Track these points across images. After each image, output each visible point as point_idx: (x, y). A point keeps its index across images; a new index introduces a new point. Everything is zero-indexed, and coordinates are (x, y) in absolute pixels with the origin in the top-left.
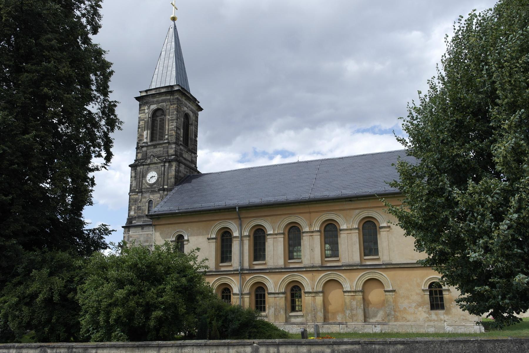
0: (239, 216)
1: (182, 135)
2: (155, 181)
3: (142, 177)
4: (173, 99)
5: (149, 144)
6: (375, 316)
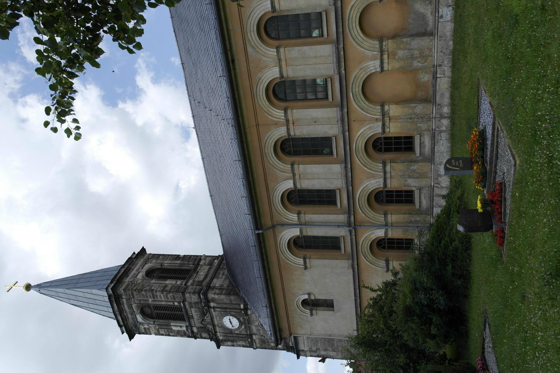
1: (174, 282)
2: (235, 319)
3: (232, 333)
4: (126, 295)
5: (187, 324)
6: (424, 16)
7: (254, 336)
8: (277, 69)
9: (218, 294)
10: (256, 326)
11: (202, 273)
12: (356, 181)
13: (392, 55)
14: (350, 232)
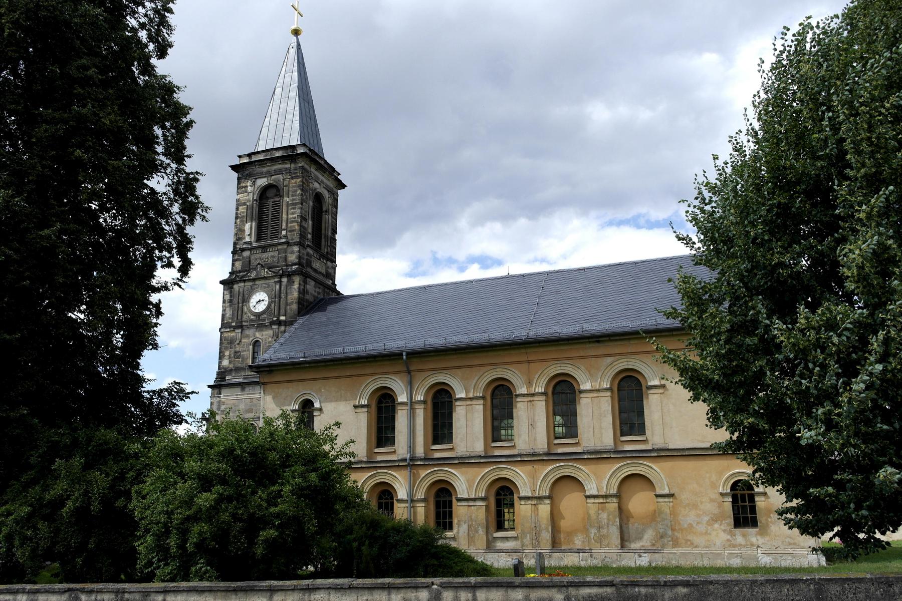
0: (408, 368)
1: (310, 231)
2: (264, 307)
4: (295, 169)
5: (254, 245)
6: (640, 538)
7: (240, 330)
9: (299, 288)
12: (464, 469)
14: (405, 460)
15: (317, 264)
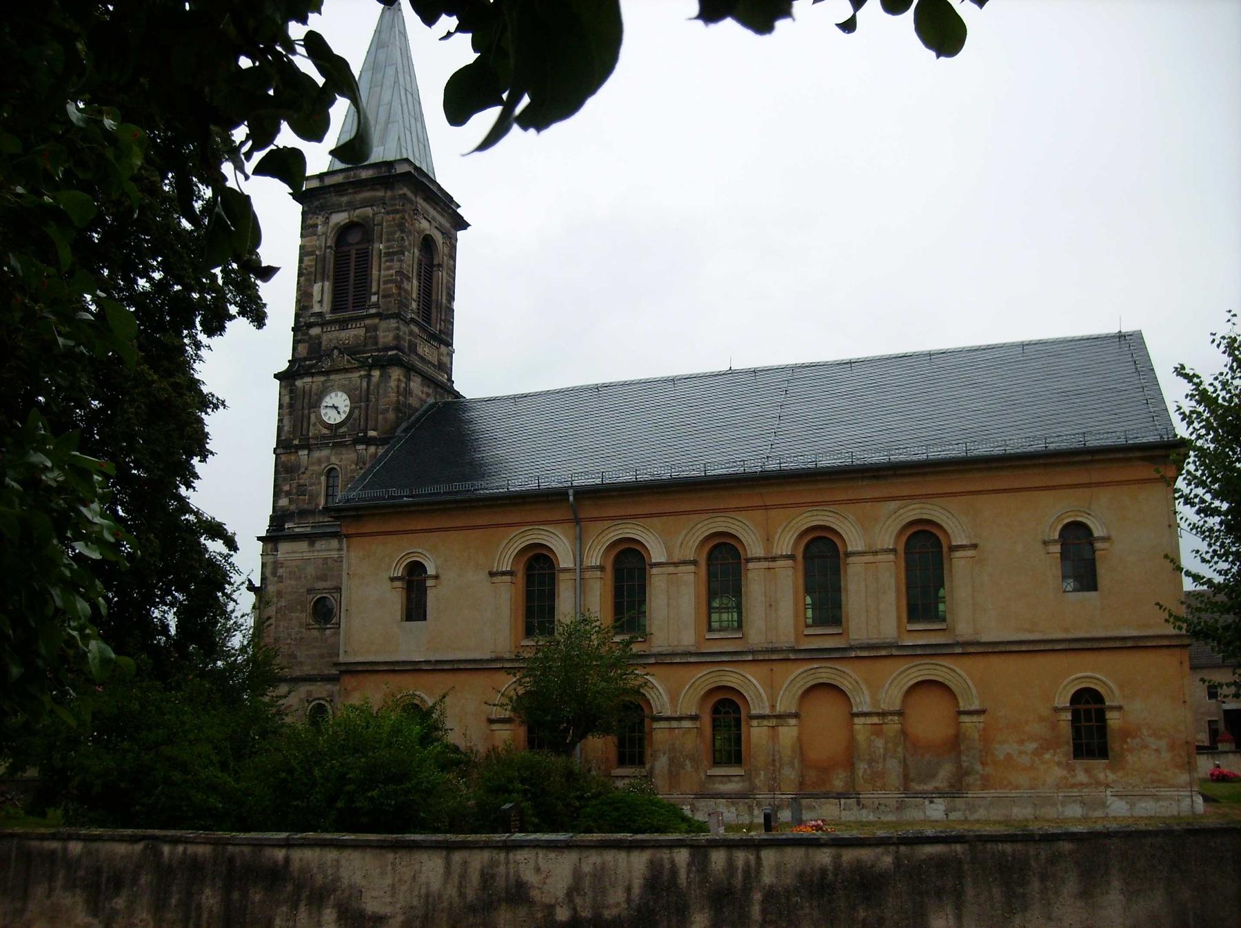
0: (575, 514)
1: (414, 296)
4: (393, 198)
5: (328, 317)
6: (933, 776)
7: (306, 452)
8: (860, 548)
9: (398, 387)
10: (328, 458)
11: (426, 350)
13: (877, 730)
15: (424, 350)
